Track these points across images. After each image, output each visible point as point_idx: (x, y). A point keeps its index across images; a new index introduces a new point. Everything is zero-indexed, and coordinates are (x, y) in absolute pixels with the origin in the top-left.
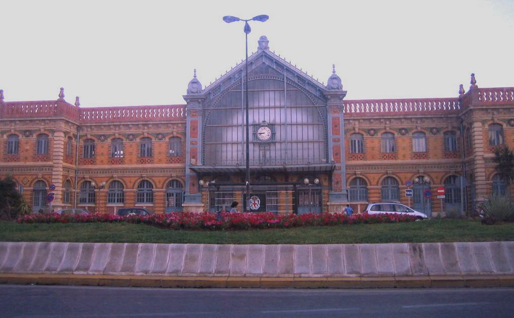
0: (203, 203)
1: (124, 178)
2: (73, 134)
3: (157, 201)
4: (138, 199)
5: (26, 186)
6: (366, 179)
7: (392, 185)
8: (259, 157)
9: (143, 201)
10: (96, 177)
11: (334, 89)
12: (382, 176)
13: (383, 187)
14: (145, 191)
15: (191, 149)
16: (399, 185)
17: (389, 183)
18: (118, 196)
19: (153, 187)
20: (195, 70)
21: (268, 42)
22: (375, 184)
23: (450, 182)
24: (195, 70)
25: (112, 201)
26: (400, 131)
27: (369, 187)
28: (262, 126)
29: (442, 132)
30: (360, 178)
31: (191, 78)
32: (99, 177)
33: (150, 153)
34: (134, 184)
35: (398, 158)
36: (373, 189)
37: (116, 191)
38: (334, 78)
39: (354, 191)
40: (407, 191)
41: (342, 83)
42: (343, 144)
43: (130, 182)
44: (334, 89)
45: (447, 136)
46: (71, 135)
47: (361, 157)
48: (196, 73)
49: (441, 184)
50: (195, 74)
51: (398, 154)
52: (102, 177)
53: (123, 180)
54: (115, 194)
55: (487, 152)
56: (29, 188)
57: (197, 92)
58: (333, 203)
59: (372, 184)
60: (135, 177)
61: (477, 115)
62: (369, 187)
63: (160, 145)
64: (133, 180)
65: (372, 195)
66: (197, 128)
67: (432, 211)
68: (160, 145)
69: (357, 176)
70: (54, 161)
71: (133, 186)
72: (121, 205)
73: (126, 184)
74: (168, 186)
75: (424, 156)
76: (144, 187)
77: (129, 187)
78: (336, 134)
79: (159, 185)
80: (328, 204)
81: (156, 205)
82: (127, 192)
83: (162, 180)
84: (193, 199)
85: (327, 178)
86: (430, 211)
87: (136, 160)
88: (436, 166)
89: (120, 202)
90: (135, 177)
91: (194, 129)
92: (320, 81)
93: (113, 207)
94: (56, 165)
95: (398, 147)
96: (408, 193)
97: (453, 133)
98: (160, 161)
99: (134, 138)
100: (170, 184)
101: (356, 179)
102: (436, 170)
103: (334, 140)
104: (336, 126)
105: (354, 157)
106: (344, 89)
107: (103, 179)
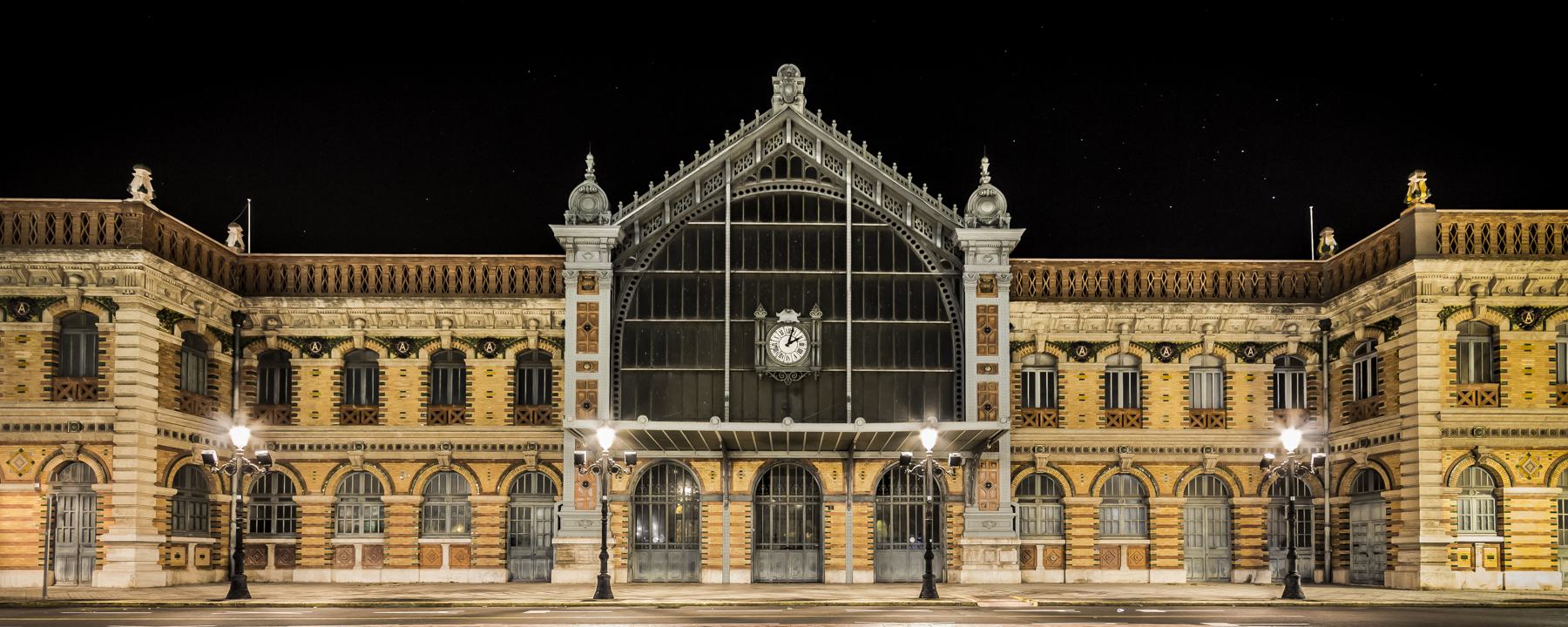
4: (528, 517)
5: (1535, 480)
6: (1062, 479)
9: (268, 530)
12: (509, 470)
13: (1104, 501)
14: (189, 494)
18: (280, 515)
19: (295, 493)
22: (1170, 490)
23: (1366, 489)
25: (261, 530)
27: (1236, 500)
29: (1269, 357)
33: (1052, 400)
42: (1004, 382)
47: (1049, 420)
53: (1062, 472)
55: (1098, 424)
56: (1545, 490)
59: (1077, 492)
61: (83, 308)
62: (1068, 499)
63: (1082, 377)
65: (1075, 521)
67: (1234, 567)
69: (82, 458)
70: (120, 401)
71: (411, 487)
72: (377, 540)
74: (512, 492)
76: (1033, 492)
77: (398, 489)
80: (963, 542)
81: (393, 541)
82: (1071, 506)
83: (1178, 470)
85: (718, 472)
91: (587, 328)
94: (123, 414)
97: (1297, 363)
99: (1173, 355)
100: (521, 481)
104: (987, 330)
105: (1029, 420)
107: (319, 465)
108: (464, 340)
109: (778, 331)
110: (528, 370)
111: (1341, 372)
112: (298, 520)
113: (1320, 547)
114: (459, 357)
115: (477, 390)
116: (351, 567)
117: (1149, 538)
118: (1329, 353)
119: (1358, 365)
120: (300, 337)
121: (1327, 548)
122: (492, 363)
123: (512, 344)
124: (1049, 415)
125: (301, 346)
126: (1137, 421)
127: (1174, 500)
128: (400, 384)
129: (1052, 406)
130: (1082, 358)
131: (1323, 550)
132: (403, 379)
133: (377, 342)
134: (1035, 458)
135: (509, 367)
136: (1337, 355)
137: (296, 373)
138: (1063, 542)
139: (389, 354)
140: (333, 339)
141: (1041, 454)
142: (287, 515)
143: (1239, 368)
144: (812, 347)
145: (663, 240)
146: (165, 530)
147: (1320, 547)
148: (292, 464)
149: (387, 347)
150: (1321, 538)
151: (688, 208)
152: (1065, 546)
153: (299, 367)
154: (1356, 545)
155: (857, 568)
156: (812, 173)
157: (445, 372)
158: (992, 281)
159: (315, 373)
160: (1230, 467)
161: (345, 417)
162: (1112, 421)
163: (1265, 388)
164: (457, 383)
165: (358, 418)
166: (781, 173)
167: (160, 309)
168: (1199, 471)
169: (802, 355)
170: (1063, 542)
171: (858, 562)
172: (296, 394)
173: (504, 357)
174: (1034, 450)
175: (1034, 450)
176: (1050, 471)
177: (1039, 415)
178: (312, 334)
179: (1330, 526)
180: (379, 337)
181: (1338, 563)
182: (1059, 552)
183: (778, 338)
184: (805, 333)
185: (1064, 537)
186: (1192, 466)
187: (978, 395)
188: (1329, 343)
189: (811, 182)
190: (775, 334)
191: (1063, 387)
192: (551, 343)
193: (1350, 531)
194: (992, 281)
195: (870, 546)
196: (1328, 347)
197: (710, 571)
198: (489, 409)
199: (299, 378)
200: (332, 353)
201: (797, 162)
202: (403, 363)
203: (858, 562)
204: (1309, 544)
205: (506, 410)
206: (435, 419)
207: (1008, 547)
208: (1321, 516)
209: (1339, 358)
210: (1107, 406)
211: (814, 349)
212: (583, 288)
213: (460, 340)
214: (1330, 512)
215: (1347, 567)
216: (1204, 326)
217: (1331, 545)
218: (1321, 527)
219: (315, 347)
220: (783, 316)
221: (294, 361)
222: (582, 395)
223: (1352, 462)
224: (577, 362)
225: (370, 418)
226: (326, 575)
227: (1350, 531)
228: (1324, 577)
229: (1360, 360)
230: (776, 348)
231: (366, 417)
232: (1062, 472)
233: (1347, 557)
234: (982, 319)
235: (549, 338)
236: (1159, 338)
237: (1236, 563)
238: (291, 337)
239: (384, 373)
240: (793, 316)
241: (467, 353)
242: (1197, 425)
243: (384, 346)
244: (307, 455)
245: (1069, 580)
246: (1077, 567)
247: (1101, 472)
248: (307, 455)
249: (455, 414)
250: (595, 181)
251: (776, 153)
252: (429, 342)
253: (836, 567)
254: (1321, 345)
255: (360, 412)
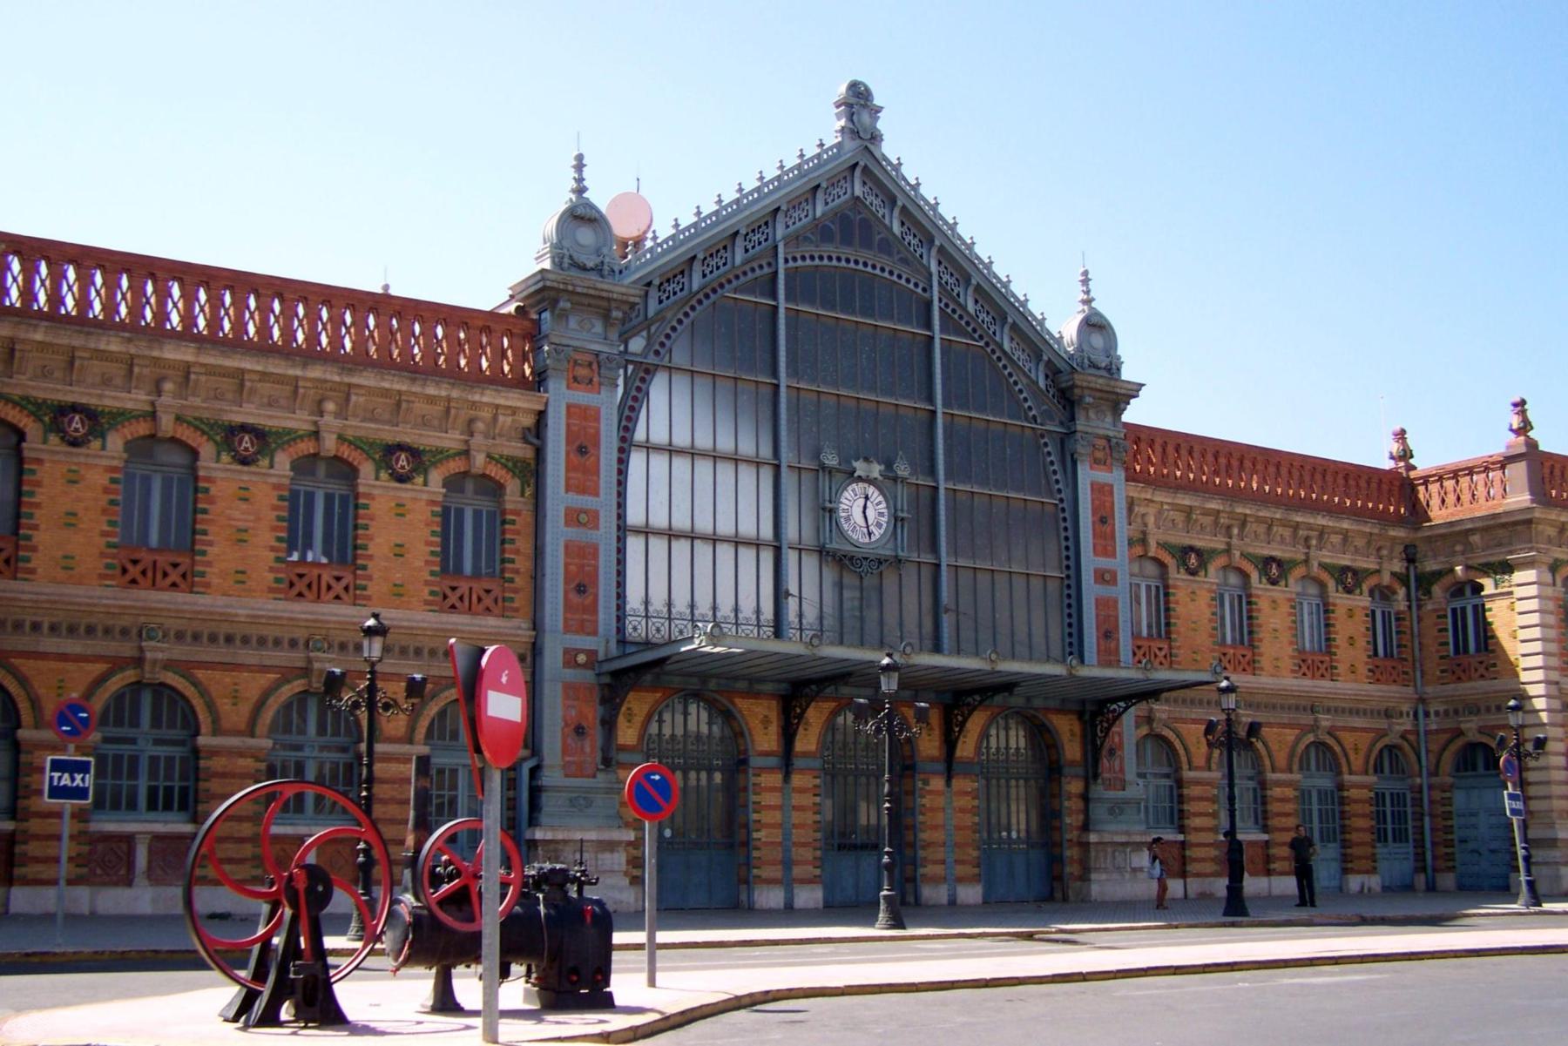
0: (627, 825)
1: (200, 674)
2: (1394, 574)
3: (1197, 822)
6: (198, 703)
7: (158, 734)
8: (758, 611)
10: (1344, 729)
11: (1099, 368)
12: (1449, 742)
15: (174, 398)
16: (197, 733)
17: (312, 728)
18: (153, 774)
20: (580, 158)
21: (879, 110)
24: (580, 158)
26: (54, 420)
28: (860, 479)
30: (160, 688)
31: (562, 200)
32: (43, 656)
34: (260, 705)
35: (207, 585)
36: (1198, 782)
37: (141, 743)
38: (1095, 325)
39: (118, 759)
40: (57, 766)
41: (1119, 352)
43: (235, 698)
44: (1099, 368)
45: (304, 486)
46: (1386, 579)
48: (586, 173)
49: (1366, 773)
50: (580, 180)
51: (34, 549)
52: (64, 657)
53: (196, 684)
54: (134, 760)
55: (427, 603)
57: (598, 269)
58: (1107, 838)
60: (264, 669)
64: (253, 685)
66: (597, 445)
67: (1345, 871)
68: (400, 510)
73: (211, 707)
75: (1323, 667)
76: (135, 723)
77: (226, 724)
78: (582, 490)
79: (235, 715)
82: (214, 752)
84: (580, 803)
86: (1335, 867)
87: (271, 576)
88: (630, 403)
89: (168, 807)
90: (264, 669)
92: (1053, 326)
93: (129, 839)
95: (1260, 626)
96: (66, 780)
98: (1276, 671)
101: (137, 686)
102: (1359, 722)
103: (573, 517)
106: (1127, 374)
107: (70, 666)
108: (355, 444)
109: (850, 488)
110: (456, 509)
111: (1435, 615)
112: (1186, 807)
113: (1419, 844)
114: (345, 471)
115: (378, 540)
116: (129, 883)
117: (1182, 832)
118: (1417, 590)
119: (1454, 611)
120: (45, 401)
121: (1428, 845)
122: (405, 492)
123: (440, 461)
124: (338, 579)
125: (46, 419)
126: (184, 576)
127: (1205, 775)
128: (237, 514)
129: (343, 560)
130: (245, 457)
131: (1423, 847)
132: (244, 506)
133: (197, 428)
134: (141, 649)
135: (433, 503)
136: (1428, 593)
137: (33, 472)
138: (1181, 837)
139: (219, 454)
140: (110, 413)
141: (153, 643)
142: (117, 774)
143: (1340, 600)
144: (896, 520)
145: (686, 314)
146: (810, 822)
147: (1419, 844)
148: (16, 661)
149: (216, 442)
150: (1420, 830)
151: (723, 269)
152: (1183, 843)
153: (39, 461)
154: (1463, 841)
155: (960, 880)
156: (886, 246)
157: (310, 498)
158: (590, 364)
159: (73, 477)
160: (16, 661)
161: (124, 571)
162: (299, 585)
163: (1207, 613)
164: (455, 547)
165: (150, 574)
166: (847, 241)
167: (1551, 561)
168: (130, 675)
169: (882, 531)
170: (1181, 837)
171: (961, 870)
172: (31, 516)
173: (425, 484)
174: (140, 635)
175: (140, 635)
176: (171, 679)
177: (319, 576)
178: (70, 398)
179: (1432, 816)
180: (201, 420)
181: (1441, 864)
182: (1175, 851)
183: (878, 509)
184: (884, 496)
185: (1182, 829)
186: (118, 664)
187: (1097, 616)
188: (1416, 576)
189: (883, 260)
190: (846, 494)
191: (205, 511)
192: (504, 466)
193: (1454, 822)
194: (590, 364)
195: (818, 844)
196: (1416, 580)
197: (765, 887)
198: (398, 577)
199: (38, 484)
200: (277, 459)
201: (866, 226)
202: (245, 474)
203: (961, 870)
204: (1407, 841)
205: (427, 583)
206: (449, 602)
207: (1138, 846)
208: (1418, 802)
209: (1430, 598)
210: (444, 570)
211: (899, 524)
212: (575, 379)
213: (350, 443)
214: (1429, 796)
215: (1452, 869)
216: (471, 421)
217: (1526, 840)
218: (1419, 817)
219: (77, 424)
220: (860, 467)
221: (31, 447)
222: (573, 568)
223: (1460, 733)
224: (567, 509)
225: (174, 576)
226: (82, 898)
227: (1454, 822)
228: (1427, 882)
229: (1457, 604)
230: (848, 519)
231: (165, 575)
232: (196, 684)
233: (1449, 857)
234: (1097, 502)
235: (501, 456)
236: (390, 434)
237: (1350, 865)
238: (26, 398)
239: (207, 490)
240: (876, 470)
241: (360, 468)
242: (300, 595)
243: (210, 438)
244: (50, 644)
245: (1191, 893)
246: (1198, 875)
247: (276, 686)
248: (50, 644)
249: (333, 583)
250: (292, 462)
251: (840, 206)
252: (294, 440)
253: (935, 880)
254: (1408, 576)
255: (155, 563)
